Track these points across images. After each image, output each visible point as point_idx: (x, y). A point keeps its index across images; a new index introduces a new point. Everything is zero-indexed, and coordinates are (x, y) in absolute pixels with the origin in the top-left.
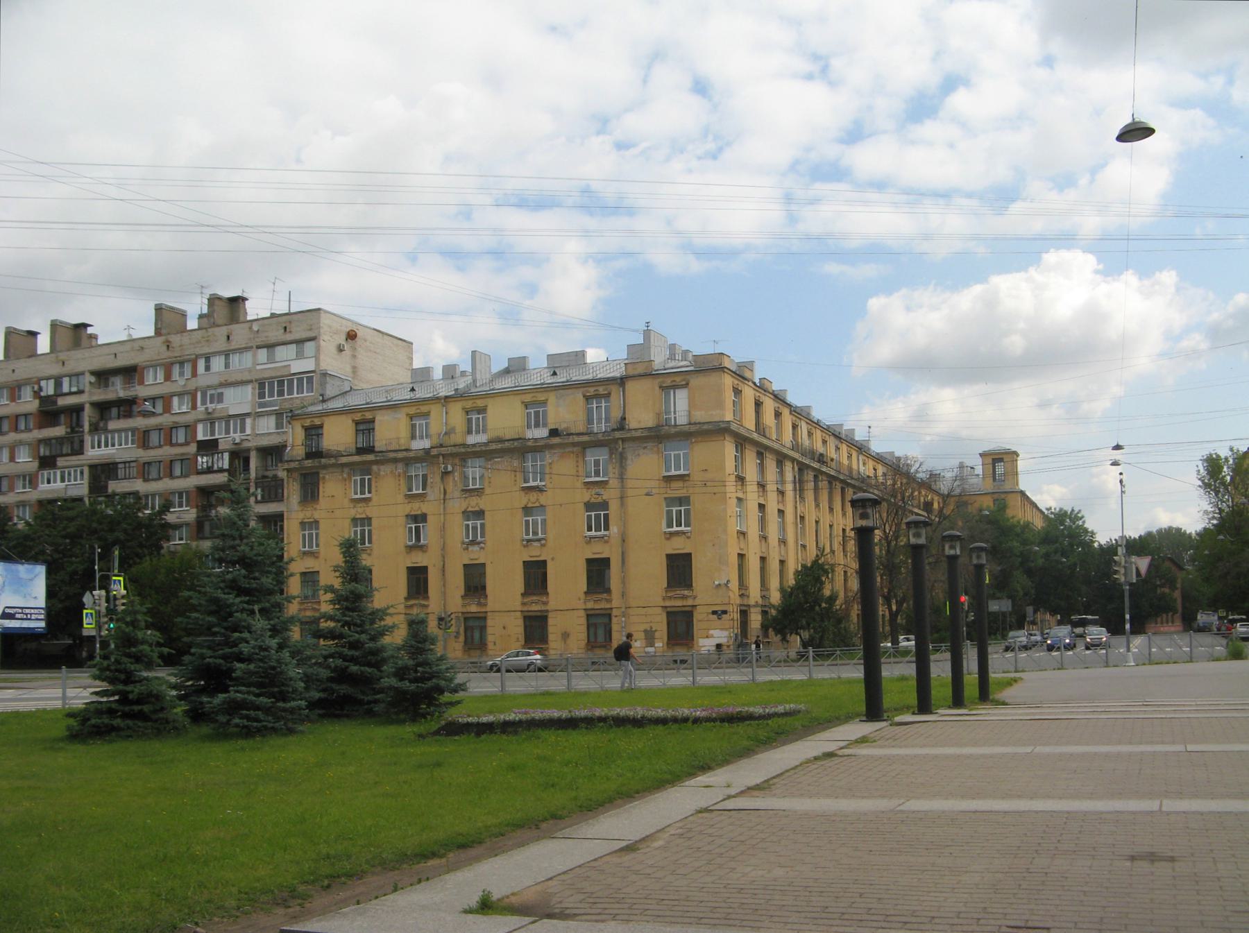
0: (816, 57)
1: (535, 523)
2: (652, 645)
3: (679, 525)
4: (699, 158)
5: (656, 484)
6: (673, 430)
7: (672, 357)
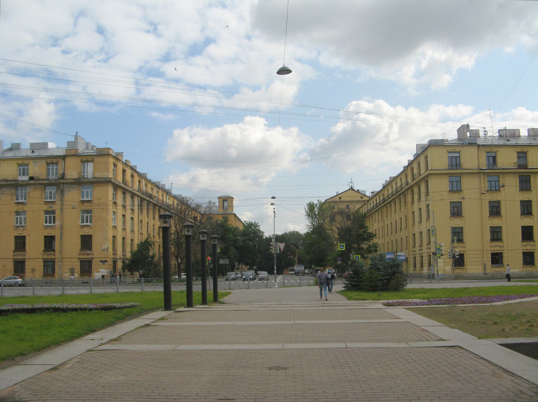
0: (152, 23)
1: (21, 219)
2: (73, 275)
3: (87, 222)
4: (99, 61)
5: (77, 204)
6: (86, 181)
7: (87, 148)
